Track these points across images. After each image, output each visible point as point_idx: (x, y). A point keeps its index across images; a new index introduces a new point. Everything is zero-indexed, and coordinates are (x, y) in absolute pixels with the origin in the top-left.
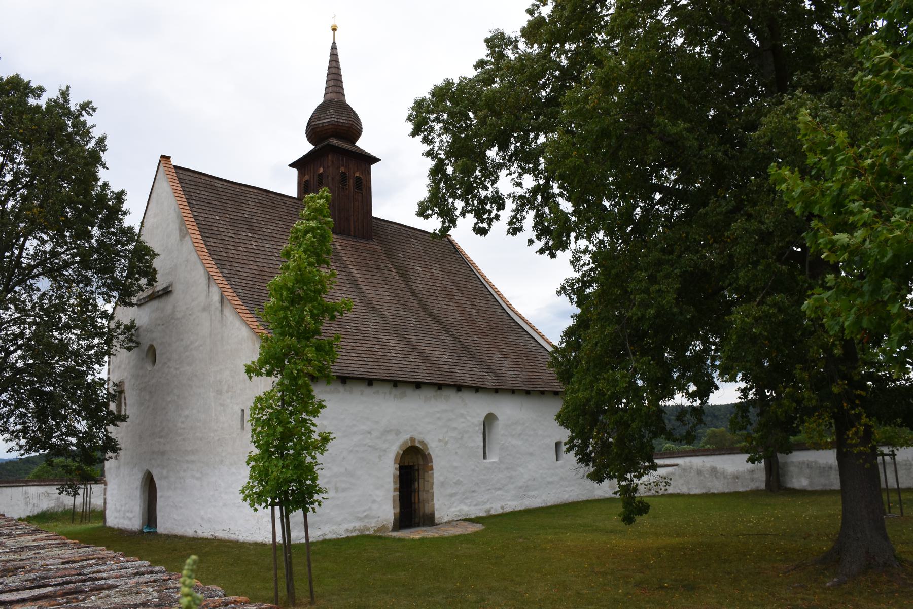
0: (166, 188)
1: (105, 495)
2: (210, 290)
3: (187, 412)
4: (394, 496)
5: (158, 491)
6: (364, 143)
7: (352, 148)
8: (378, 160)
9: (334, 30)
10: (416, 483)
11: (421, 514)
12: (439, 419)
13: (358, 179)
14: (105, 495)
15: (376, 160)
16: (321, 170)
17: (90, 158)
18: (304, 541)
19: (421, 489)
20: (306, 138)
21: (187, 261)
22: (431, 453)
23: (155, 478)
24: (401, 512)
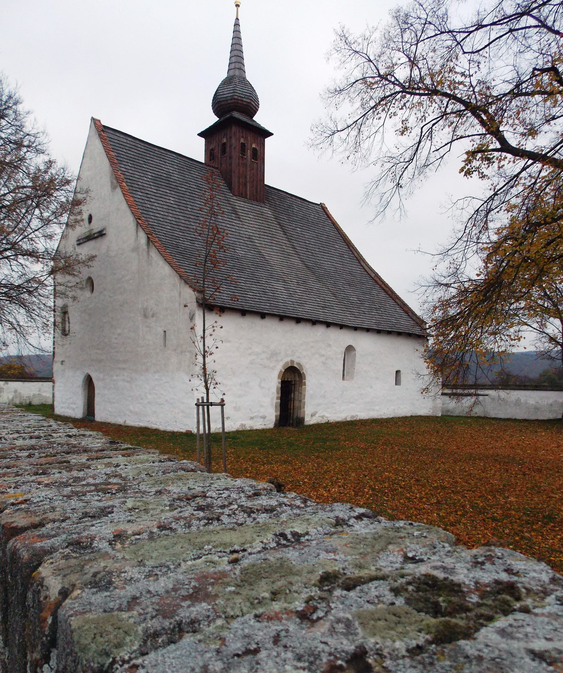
0: (98, 144)
1: (53, 390)
2: (139, 233)
3: (119, 331)
4: (276, 403)
5: (96, 389)
6: (260, 119)
7: (250, 123)
8: (271, 134)
9: (237, 6)
11: (295, 417)
12: (312, 347)
13: (255, 151)
14: (53, 390)
15: (270, 134)
16: (225, 141)
18: (221, 430)
20: (211, 108)
21: (118, 209)
22: (305, 372)
23: (94, 380)
24: (280, 415)
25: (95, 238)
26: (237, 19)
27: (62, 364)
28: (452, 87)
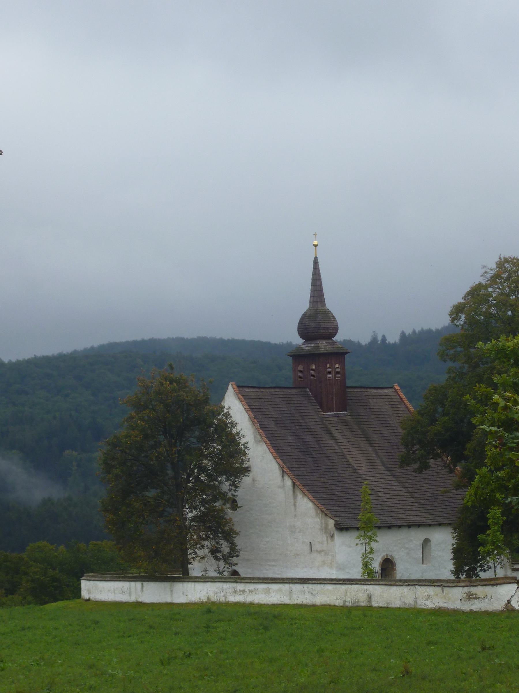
3: (268, 540)
28: (499, 355)
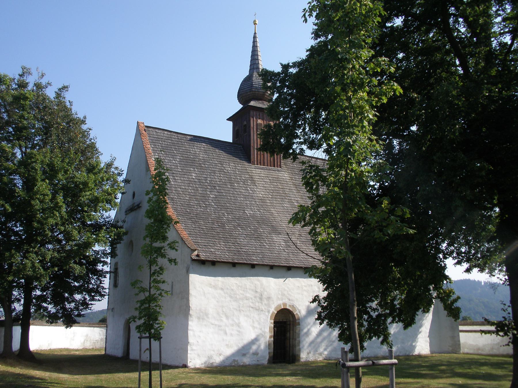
10: (288, 333)
11: (291, 354)
17: (443, 60)
18: (153, 372)
19: (291, 337)
25: (135, 210)
26: (255, 33)
27: (112, 311)
